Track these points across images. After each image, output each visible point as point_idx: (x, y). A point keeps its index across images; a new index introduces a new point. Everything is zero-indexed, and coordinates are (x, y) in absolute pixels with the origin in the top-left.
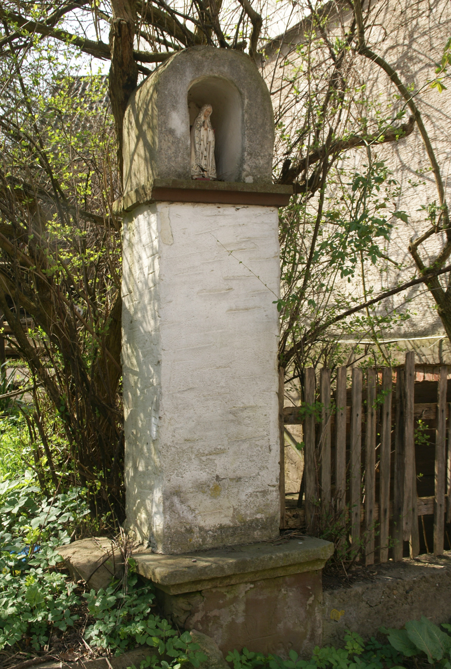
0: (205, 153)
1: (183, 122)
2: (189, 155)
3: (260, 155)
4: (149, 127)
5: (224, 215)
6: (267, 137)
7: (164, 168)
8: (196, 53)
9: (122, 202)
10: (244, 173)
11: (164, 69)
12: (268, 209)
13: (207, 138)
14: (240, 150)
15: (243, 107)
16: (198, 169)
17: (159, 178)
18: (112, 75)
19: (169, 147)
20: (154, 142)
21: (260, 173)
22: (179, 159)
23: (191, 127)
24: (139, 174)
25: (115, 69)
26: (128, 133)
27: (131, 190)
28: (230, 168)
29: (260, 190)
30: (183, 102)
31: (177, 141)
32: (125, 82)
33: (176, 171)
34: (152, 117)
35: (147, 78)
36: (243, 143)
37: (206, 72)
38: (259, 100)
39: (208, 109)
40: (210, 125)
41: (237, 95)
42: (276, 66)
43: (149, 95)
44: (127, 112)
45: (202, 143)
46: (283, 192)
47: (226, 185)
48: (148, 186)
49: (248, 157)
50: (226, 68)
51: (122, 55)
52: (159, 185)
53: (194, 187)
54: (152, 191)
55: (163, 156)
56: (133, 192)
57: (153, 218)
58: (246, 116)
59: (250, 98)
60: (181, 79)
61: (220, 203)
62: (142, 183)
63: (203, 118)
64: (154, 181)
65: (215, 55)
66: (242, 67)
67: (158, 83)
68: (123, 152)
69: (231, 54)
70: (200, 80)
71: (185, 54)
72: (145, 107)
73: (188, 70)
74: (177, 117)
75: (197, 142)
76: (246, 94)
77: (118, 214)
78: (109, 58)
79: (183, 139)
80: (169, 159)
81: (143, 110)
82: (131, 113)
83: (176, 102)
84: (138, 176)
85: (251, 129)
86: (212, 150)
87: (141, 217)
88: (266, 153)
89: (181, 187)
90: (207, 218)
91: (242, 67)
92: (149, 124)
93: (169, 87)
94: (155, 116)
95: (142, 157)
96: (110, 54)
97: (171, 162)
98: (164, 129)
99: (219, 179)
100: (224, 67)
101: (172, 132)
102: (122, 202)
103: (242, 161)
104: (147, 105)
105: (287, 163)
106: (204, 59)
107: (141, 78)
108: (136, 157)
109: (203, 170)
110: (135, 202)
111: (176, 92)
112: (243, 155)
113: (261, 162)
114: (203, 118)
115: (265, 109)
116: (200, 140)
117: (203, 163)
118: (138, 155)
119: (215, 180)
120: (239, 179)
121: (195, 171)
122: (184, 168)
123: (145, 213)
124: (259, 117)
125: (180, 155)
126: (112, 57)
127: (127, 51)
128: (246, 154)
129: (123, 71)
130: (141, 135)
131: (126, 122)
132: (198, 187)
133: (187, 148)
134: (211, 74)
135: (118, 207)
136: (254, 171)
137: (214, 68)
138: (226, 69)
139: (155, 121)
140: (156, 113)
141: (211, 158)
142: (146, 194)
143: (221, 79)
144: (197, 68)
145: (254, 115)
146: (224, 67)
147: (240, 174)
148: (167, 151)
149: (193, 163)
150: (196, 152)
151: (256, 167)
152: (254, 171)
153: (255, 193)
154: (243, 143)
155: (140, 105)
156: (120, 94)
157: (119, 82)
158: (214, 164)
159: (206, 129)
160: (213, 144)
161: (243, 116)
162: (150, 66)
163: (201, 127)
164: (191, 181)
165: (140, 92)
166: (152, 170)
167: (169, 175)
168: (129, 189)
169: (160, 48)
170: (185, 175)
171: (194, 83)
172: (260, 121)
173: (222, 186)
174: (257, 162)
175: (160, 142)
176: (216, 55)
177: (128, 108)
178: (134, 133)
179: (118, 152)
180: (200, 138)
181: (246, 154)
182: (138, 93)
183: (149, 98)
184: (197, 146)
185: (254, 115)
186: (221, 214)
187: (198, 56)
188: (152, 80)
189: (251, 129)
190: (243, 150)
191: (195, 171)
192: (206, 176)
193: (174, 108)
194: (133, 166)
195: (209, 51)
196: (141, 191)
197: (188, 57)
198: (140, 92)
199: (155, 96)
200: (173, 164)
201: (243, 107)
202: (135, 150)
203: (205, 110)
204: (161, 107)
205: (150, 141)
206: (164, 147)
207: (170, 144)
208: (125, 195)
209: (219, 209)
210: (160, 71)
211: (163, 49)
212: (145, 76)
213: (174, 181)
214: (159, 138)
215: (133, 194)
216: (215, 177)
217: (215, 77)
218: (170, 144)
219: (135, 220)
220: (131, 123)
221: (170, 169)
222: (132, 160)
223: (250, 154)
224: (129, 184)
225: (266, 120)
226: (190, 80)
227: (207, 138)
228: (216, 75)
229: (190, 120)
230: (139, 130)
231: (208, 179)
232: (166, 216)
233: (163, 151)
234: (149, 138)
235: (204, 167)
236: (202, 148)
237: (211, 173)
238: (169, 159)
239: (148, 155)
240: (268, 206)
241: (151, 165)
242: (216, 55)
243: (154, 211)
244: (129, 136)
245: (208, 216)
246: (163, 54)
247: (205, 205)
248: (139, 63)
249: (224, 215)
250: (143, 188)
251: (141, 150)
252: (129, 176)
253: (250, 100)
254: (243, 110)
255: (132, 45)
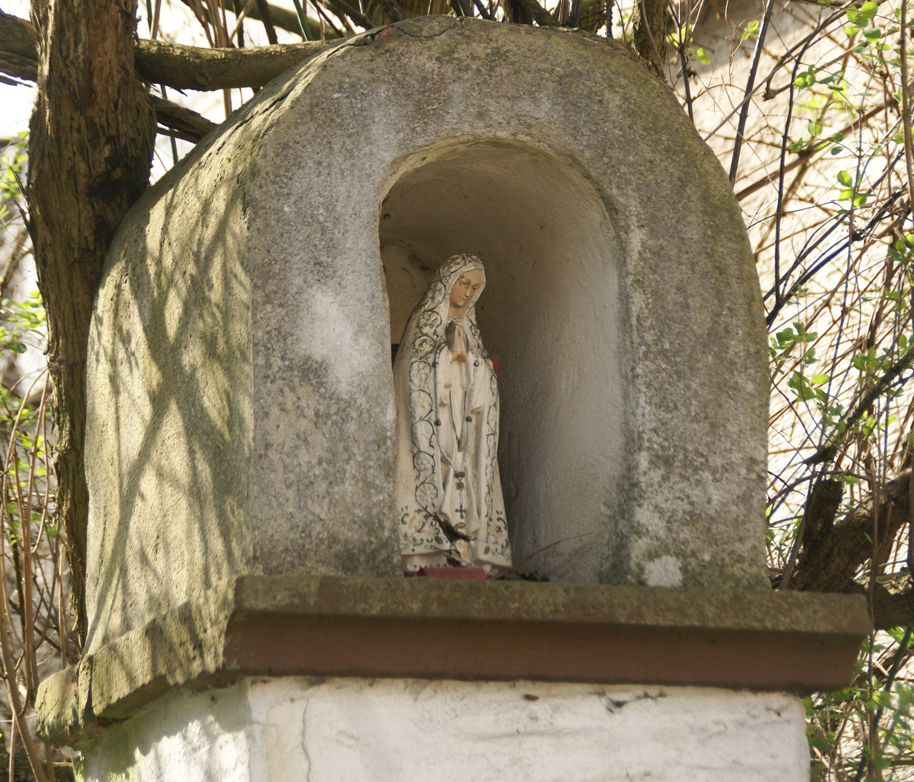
0: (458, 460)
1: (360, 330)
2: (390, 469)
3: (706, 465)
4: (211, 353)
5: (558, 734)
6: (736, 388)
7: (279, 530)
8: (415, 47)
9: (83, 679)
10: (639, 547)
11: (275, 115)
12: (759, 701)
13: (467, 395)
14: (616, 443)
15: (622, 264)
16: (430, 530)
17: (259, 572)
18: (42, 139)
19: (303, 439)
20: (234, 419)
21: (713, 541)
22: (349, 488)
23: (395, 348)
24: (163, 552)
25: (55, 119)
26: (114, 379)
27: (127, 626)
28: (574, 520)
29: (713, 616)
30: (360, 247)
31: (334, 413)
32: (101, 168)
33: (334, 539)
34: (227, 315)
35: (193, 157)
36: (628, 414)
37: (458, 124)
38: (693, 233)
39: (466, 275)
40: (475, 341)
41: (595, 214)
42: (749, 90)
43: (213, 222)
44: (105, 294)
45: (444, 416)
46: (823, 627)
47: (562, 597)
48: (212, 608)
49: (656, 475)
50: (546, 105)
51: (89, 62)
52: (261, 604)
53: (415, 607)
54: (230, 631)
55: (277, 478)
56: (136, 635)
57: (231, 750)
58: (638, 301)
59: (651, 223)
60: (350, 154)
61: (535, 678)
62: (180, 599)
63: (444, 312)
64: (240, 585)
65: (497, 52)
66: (614, 100)
67: (254, 172)
68: (88, 461)
69: (562, 47)
70: (431, 157)
71: (367, 54)
72: (191, 269)
73: (378, 115)
74: (334, 310)
75: (420, 412)
76: (634, 207)
77: (58, 736)
78: (33, 76)
79: (362, 400)
80: (304, 486)
81: (182, 285)
82: (127, 294)
83: (332, 247)
84: (159, 565)
85: (664, 353)
86: (489, 444)
87: (170, 746)
88: (736, 457)
89: (360, 608)
90: (481, 747)
91: (614, 100)
92: (210, 343)
93: (298, 186)
94: (237, 310)
95: (176, 483)
96: (35, 59)
97: (311, 504)
98: (277, 362)
99: (525, 570)
100: (535, 100)
101: (312, 372)
102: (83, 679)
103: (629, 491)
104: (204, 264)
105: (824, 496)
106: (448, 70)
107: (164, 156)
108: (148, 483)
109: (452, 534)
110: (143, 677)
111: (330, 207)
112: (631, 468)
113: (716, 497)
114: (444, 312)
115: (721, 270)
116: (436, 404)
117: (451, 503)
118: (160, 474)
119: (503, 574)
120: (617, 570)
121: (416, 539)
122: (371, 525)
123: (194, 728)
124: (695, 302)
125: (351, 468)
126: (45, 69)
127: (109, 44)
128: (643, 461)
129: (91, 123)
130: (173, 389)
131: (101, 336)
132: (435, 610)
133: (380, 442)
134: (481, 130)
135: (63, 702)
136: (685, 534)
137: (492, 106)
138: (543, 110)
139: (240, 330)
140: (242, 294)
141: (484, 480)
142: (199, 646)
143: (522, 148)
144: (419, 107)
145: (673, 296)
146: (535, 100)
147: (621, 547)
148: (293, 453)
149: (407, 501)
150: (416, 456)
151: (693, 518)
152: (685, 534)
153: (691, 630)
154: (628, 414)
155: (168, 261)
156: (78, 218)
157: (73, 174)
158: (500, 506)
159: (461, 359)
160: (491, 420)
161: (625, 298)
162: (207, 104)
163: (436, 348)
164: (406, 583)
165: (169, 211)
166: (225, 535)
167: (302, 556)
168: (116, 621)
169: (240, 31)
170: (373, 555)
171: (405, 168)
172: (700, 321)
173: (541, 600)
174: (696, 494)
175: (262, 414)
176: (498, 55)
177: (113, 276)
178: (140, 379)
179: (63, 460)
180: (433, 396)
181: (643, 461)
182: (157, 213)
183: (209, 233)
184: (423, 430)
185: (673, 296)
186: (541, 726)
187: (421, 59)
188: (220, 160)
189: (664, 353)
190: (632, 442)
191: (416, 539)
192: (465, 560)
193: (321, 270)
194: (134, 523)
195: (468, 39)
196: (176, 632)
197: (380, 62)
198: (169, 211)
199: (239, 224)
200: (320, 510)
201: (622, 264)
202: (145, 454)
203: (453, 280)
204: (265, 273)
205: (213, 414)
206: (282, 436)
207: (304, 424)
208: (94, 647)
209: (534, 706)
210: (257, 122)
211: (256, 35)
212: (185, 147)
213: (326, 583)
214: (256, 399)
215: (135, 644)
216: (504, 560)
217: (496, 143)
218: (304, 424)
219: (143, 762)
220: (126, 339)
221: (306, 530)
222: (129, 496)
223: (663, 460)
224: (114, 600)
225: (724, 321)
226: (388, 157)
227: (467, 395)
228: (502, 134)
229: (394, 323)
230: (162, 368)
231: (475, 572)
232: (292, 738)
233: (273, 455)
234: (211, 400)
235: (455, 519)
236: (446, 436)
237: (488, 546)
238: (304, 486)
239: (205, 471)
240: (756, 688)
241: (222, 516)
242: (498, 55)
243: (237, 721)
244: (116, 391)
245: (483, 738)
246: (260, 55)
247: (467, 688)
248: (156, 90)
249: (558, 734)
250: (187, 616)
251: (174, 449)
252: (117, 563)
253: (653, 233)
254: (622, 276)
255: (131, 21)
